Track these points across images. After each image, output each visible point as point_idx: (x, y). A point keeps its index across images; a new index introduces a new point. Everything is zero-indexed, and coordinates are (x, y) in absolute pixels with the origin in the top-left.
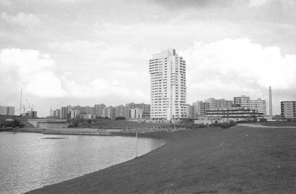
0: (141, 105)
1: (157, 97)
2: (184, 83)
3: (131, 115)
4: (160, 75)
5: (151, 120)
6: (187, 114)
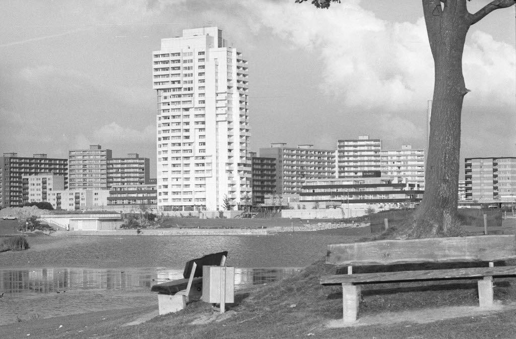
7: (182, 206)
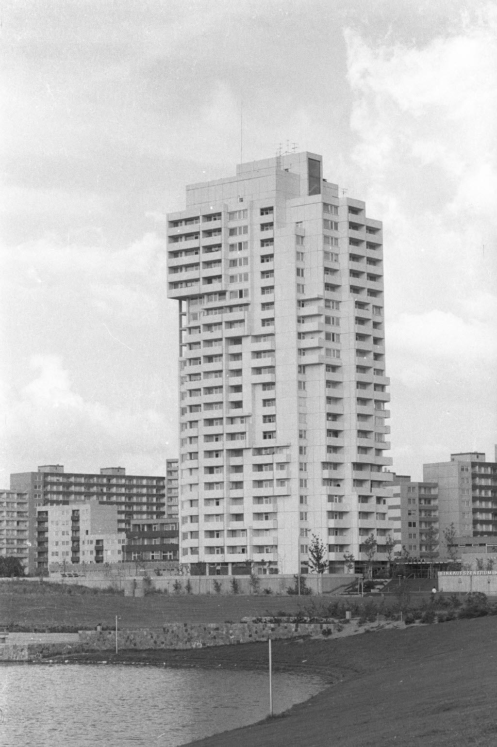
0: (109, 478)
1: (217, 437)
2: (377, 341)
3: (51, 547)
4: (231, 308)
5: (185, 577)
6: (396, 530)
7: (227, 564)
